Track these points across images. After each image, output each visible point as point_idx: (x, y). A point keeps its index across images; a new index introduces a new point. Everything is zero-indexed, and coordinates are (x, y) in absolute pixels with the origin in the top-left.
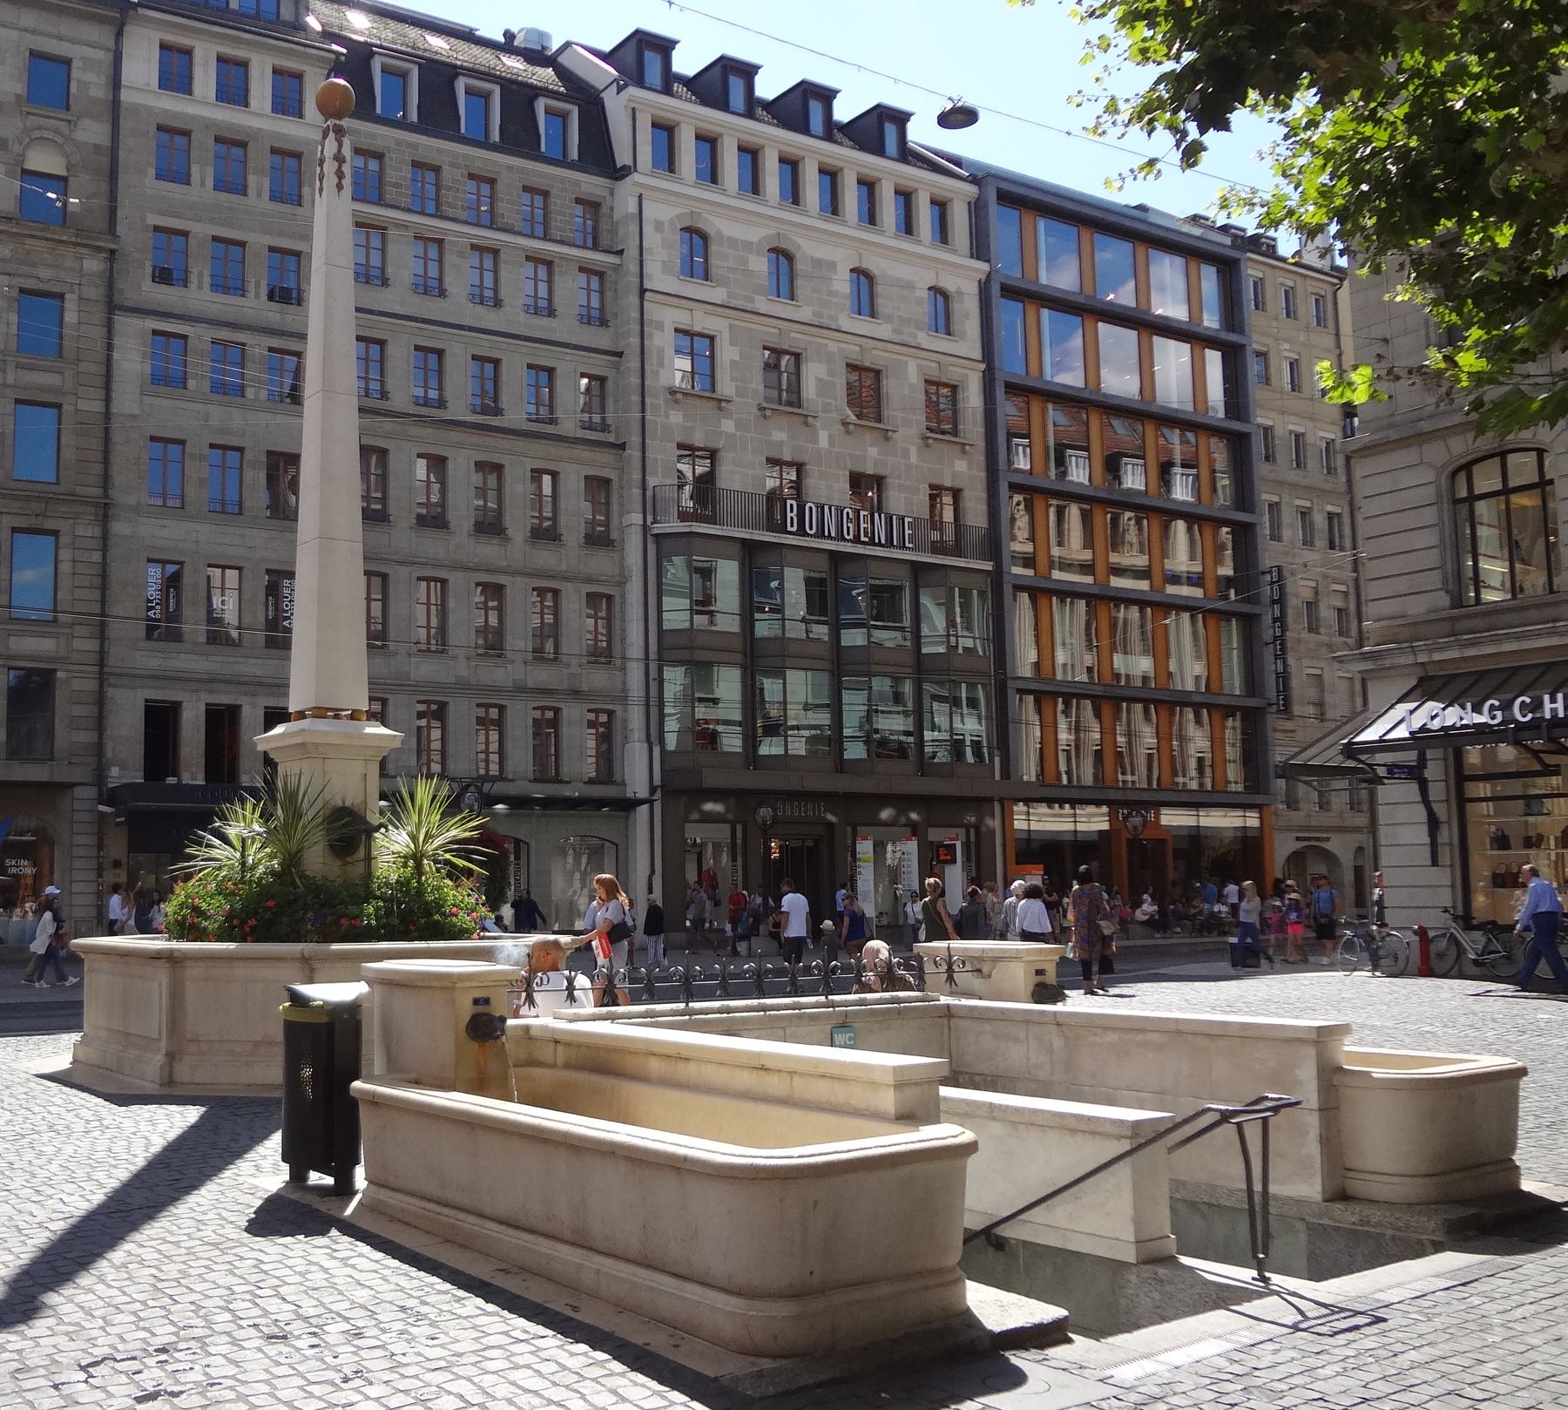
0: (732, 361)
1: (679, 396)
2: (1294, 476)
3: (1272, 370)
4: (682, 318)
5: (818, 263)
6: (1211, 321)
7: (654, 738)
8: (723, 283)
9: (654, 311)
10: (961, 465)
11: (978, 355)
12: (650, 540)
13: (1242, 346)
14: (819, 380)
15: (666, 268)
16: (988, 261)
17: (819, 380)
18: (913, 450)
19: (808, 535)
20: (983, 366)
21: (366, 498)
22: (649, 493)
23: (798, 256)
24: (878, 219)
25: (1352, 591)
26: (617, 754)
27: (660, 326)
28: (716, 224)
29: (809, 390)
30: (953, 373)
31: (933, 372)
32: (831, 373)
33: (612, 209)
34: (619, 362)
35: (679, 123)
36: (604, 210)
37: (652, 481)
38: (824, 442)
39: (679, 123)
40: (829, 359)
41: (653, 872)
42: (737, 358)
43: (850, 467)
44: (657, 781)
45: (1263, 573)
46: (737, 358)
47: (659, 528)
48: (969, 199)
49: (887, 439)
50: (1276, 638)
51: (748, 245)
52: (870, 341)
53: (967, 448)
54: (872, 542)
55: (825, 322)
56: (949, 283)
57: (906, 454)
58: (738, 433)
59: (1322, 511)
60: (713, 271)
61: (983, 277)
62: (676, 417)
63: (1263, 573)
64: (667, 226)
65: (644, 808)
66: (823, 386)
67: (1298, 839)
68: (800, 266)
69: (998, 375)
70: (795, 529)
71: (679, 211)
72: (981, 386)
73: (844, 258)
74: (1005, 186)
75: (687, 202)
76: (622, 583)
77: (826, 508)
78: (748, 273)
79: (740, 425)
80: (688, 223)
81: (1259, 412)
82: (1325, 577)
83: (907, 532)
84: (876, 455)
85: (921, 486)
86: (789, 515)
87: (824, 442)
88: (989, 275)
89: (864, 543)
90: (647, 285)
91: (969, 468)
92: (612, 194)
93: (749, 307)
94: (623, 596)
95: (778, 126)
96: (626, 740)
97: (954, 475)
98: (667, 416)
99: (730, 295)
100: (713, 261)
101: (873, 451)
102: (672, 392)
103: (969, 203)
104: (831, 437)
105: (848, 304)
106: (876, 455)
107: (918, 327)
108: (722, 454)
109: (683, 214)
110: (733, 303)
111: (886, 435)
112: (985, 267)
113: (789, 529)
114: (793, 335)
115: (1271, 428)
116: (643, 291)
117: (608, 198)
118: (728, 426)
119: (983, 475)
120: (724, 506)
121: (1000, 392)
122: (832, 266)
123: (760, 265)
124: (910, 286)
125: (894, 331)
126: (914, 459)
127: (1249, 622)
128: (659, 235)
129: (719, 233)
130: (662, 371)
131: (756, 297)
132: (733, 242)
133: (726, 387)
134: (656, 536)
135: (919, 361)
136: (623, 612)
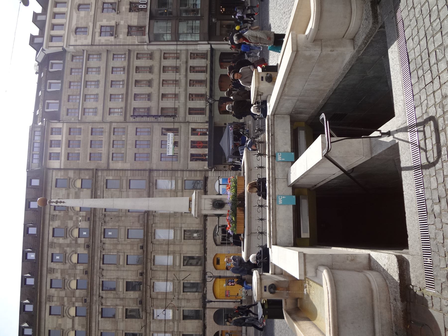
9: (96, 42)
12: (151, 44)
22: (139, 44)
27: (100, 40)
28: (74, 26)
37: (137, 43)
44: (206, 42)
51: (78, 17)
71: (71, 35)
79: (122, 19)
93: (93, 17)
94: (164, 50)
96: (197, 50)
113: (146, 7)
118: (122, 23)
131: (90, 14)
132: (77, 21)
136: (168, 50)
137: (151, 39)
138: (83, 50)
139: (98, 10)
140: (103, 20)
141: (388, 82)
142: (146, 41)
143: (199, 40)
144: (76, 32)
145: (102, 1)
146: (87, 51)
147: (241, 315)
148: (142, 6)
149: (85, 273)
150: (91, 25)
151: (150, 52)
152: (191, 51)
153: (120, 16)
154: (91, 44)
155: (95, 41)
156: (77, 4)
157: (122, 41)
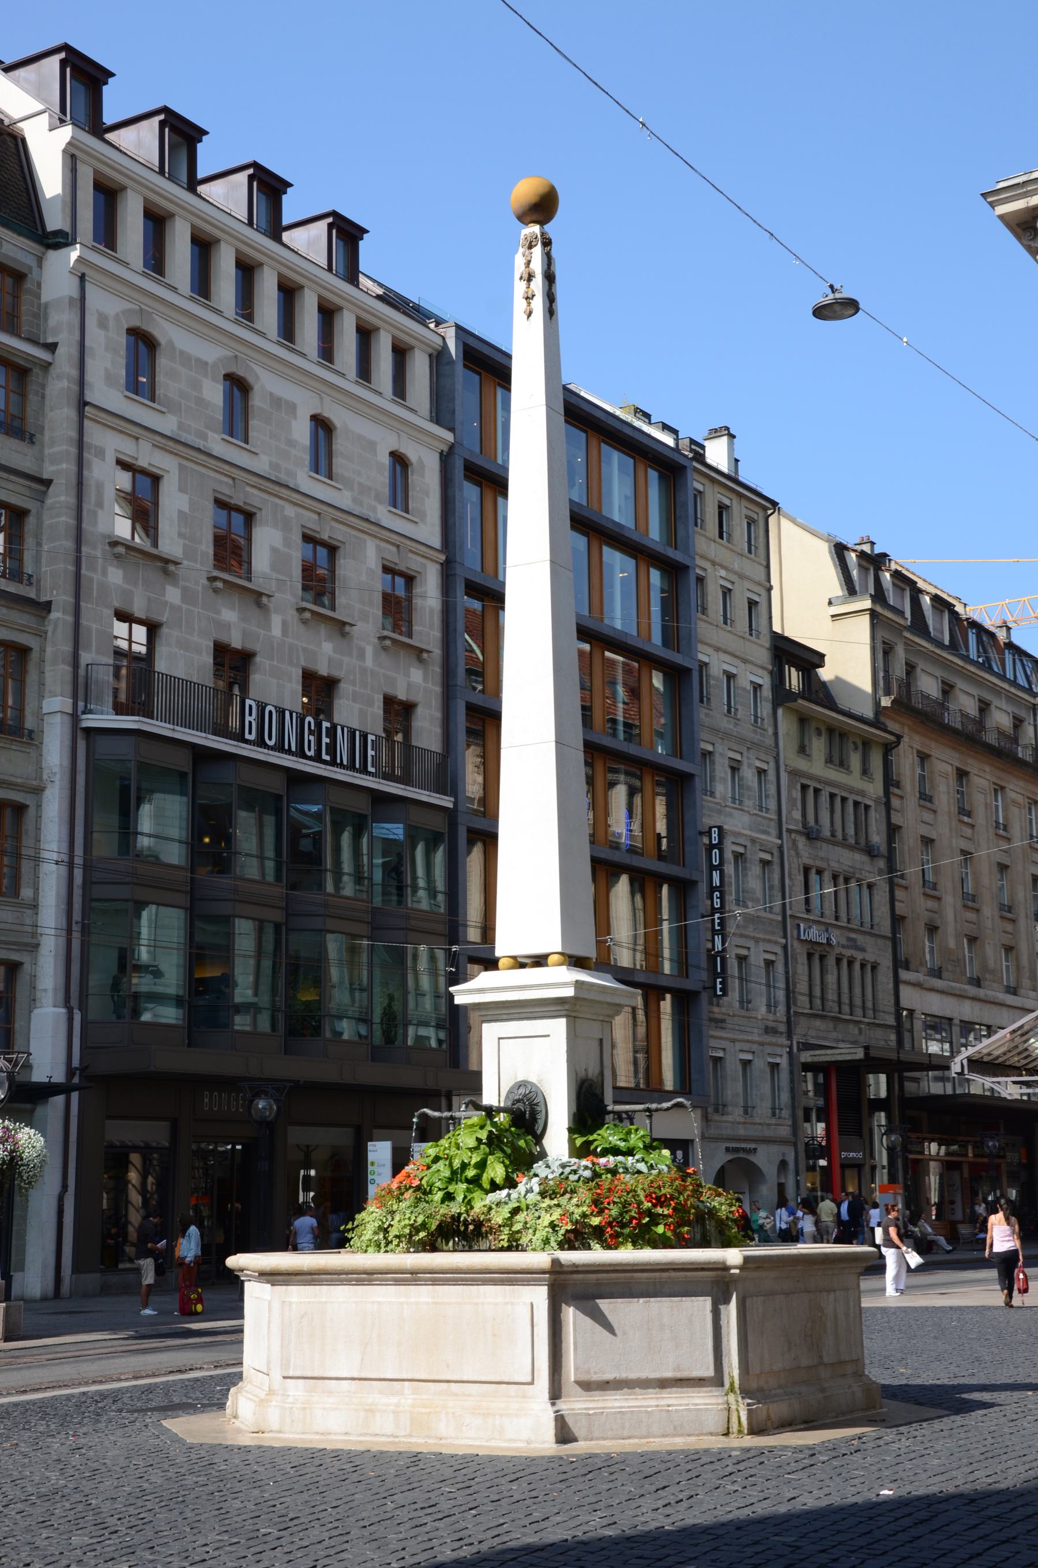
0: (180, 512)
1: (121, 550)
2: (726, 724)
3: (710, 598)
4: (128, 448)
5: (277, 402)
6: (655, 533)
7: (74, 1002)
8: (171, 407)
9: (96, 435)
10: (416, 675)
11: (436, 542)
12: (79, 734)
13: (686, 568)
14: (274, 550)
15: (109, 379)
16: (452, 429)
17: (274, 550)
18: (369, 651)
19: (247, 742)
20: (442, 558)
21: (583, 699)
22: (82, 672)
23: (256, 388)
24: (213, 289)
25: (776, 860)
26: (18, 1025)
27: (100, 453)
28: (164, 331)
29: (261, 560)
30: (412, 563)
31: (391, 555)
32: (287, 542)
33: (39, 285)
34: (45, 493)
35: (261, 265)
36: (28, 285)
37: (85, 658)
38: (276, 631)
39: (261, 265)
40: (286, 525)
41: (65, 1187)
42: (186, 509)
43: (303, 663)
44: (76, 1062)
45: (701, 833)
46: (186, 509)
47: (91, 721)
48: (431, 351)
49: (344, 635)
50: (714, 911)
51: (202, 364)
52: (330, 510)
53: (425, 655)
54: (333, 763)
55: (283, 478)
56: (412, 452)
57: (362, 655)
58: (184, 606)
59: (749, 766)
60: (160, 392)
61: (445, 449)
62: (115, 576)
63: (701, 833)
64: (111, 324)
65: (59, 1100)
66: (278, 559)
67: (728, 1149)
68: (257, 400)
69: (459, 570)
70: (252, 737)
71: (127, 306)
72: (440, 582)
73: (307, 404)
74: (471, 342)
75: (136, 295)
76: (38, 791)
77: (287, 714)
78: (200, 401)
79: (187, 595)
80: (136, 322)
81: (700, 647)
82: (753, 841)
83: (371, 753)
84: (331, 653)
85: (376, 696)
86: (248, 719)
87: (276, 631)
88: (452, 447)
89: (325, 762)
90: (88, 398)
91: (426, 680)
92: (40, 265)
93: (199, 443)
94: (39, 806)
95: (88, 132)
96: (33, 1002)
97: (409, 686)
98: (105, 573)
99: (181, 426)
100: (160, 378)
101: (327, 648)
102: (115, 543)
103: (430, 356)
104: (284, 624)
105: (307, 458)
106: (331, 653)
107: (378, 498)
108: (164, 630)
109: (130, 311)
110: (185, 437)
111: (341, 628)
112: (449, 436)
113: (247, 736)
114: (248, 489)
115: (706, 664)
116: (82, 404)
117: (35, 269)
118: (173, 595)
119: (438, 689)
120: (159, 702)
121: (460, 588)
122: (292, 408)
123: (215, 393)
124: (371, 446)
125: (355, 500)
126: (369, 662)
127: (683, 889)
128: (102, 333)
129: (170, 343)
130: (100, 512)
131: (210, 434)
132: (186, 359)
133: (170, 544)
134: (88, 731)
135: (383, 545)
136: (38, 829)
137: (103, 744)
138: (52, 347)
139: (226, 479)
140: (186, 498)
141: (1030, 1393)
142: (91, 712)
143: (91, 1017)
144: (133, 332)
145: (261, 509)
146: (47, 366)
147: (939, 1206)
148: (250, 714)
149: (34, 580)
150: (167, 424)
151: (29, 723)
152: (27, 967)
153: (200, 589)
154: (86, 404)
155: (99, 427)
156: (250, 379)
157: (95, 577)
